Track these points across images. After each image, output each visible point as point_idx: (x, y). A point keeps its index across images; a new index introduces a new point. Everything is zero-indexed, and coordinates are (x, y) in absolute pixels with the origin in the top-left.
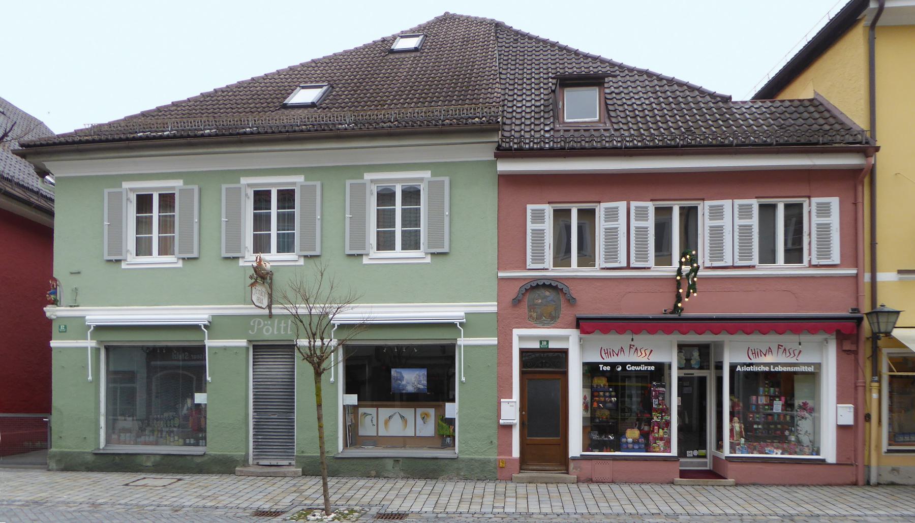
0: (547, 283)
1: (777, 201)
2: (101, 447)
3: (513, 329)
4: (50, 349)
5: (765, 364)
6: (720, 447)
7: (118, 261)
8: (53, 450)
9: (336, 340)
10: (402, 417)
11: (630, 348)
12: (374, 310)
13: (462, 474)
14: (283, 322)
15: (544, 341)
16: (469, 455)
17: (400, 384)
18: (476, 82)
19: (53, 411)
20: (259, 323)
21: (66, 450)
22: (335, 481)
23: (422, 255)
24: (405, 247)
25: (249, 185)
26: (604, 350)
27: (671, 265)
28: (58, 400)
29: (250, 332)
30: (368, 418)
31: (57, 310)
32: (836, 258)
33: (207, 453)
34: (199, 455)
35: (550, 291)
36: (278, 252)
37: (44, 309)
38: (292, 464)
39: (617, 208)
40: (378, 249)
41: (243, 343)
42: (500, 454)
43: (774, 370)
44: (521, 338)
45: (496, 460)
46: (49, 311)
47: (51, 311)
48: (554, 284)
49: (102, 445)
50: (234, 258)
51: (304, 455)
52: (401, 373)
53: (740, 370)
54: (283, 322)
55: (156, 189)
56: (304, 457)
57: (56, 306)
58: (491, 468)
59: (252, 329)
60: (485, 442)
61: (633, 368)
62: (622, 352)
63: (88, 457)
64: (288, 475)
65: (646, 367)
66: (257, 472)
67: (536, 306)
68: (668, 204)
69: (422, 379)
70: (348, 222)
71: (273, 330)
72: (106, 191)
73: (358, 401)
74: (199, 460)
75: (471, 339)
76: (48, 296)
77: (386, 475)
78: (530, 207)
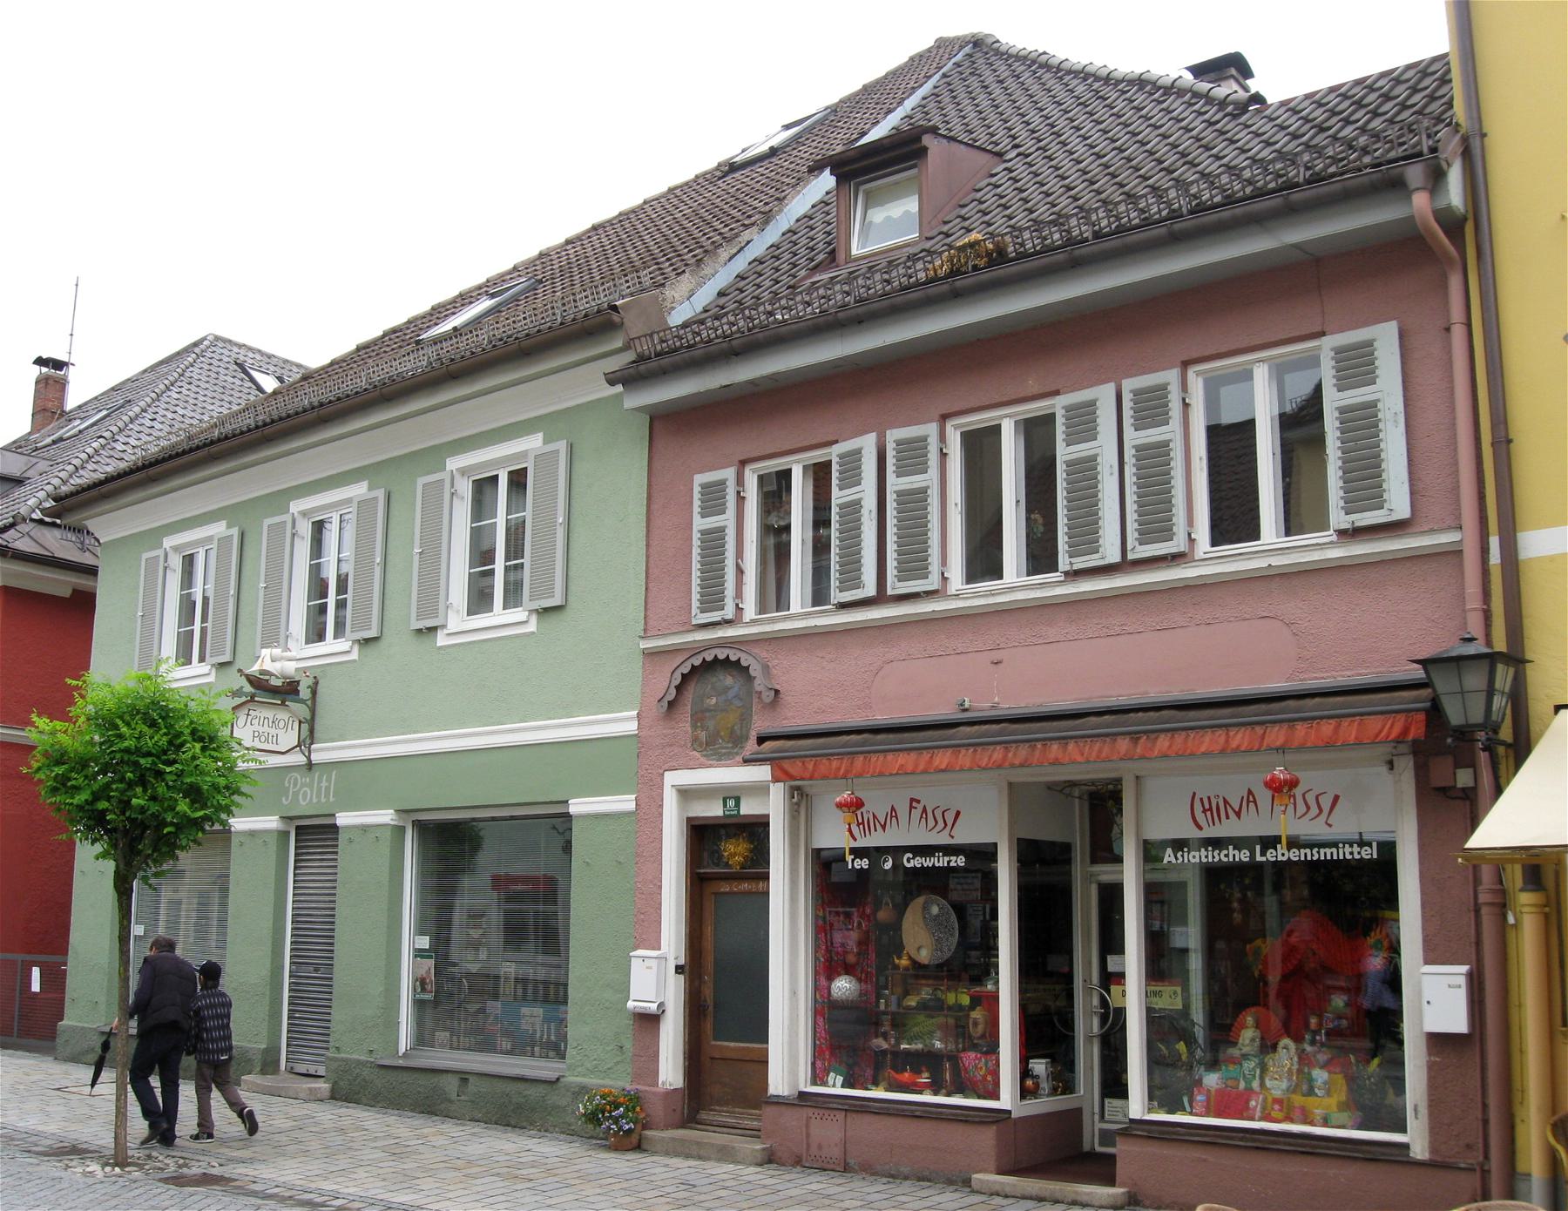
2: (402, 1050)
3: (666, 774)
5: (1239, 843)
6: (1115, 1086)
7: (433, 630)
9: (392, 811)
11: (911, 807)
26: (1201, 799)
32: (1398, 503)
34: (545, 1082)
35: (735, 673)
39: (1369, 344)
41: (386, 816)
43: (1264, 859)
44: (685, 794)
53: (1174, 861)
61: (917, 862)
62: (1252, 805)
65: (946, 859)
68: (1040, 409)
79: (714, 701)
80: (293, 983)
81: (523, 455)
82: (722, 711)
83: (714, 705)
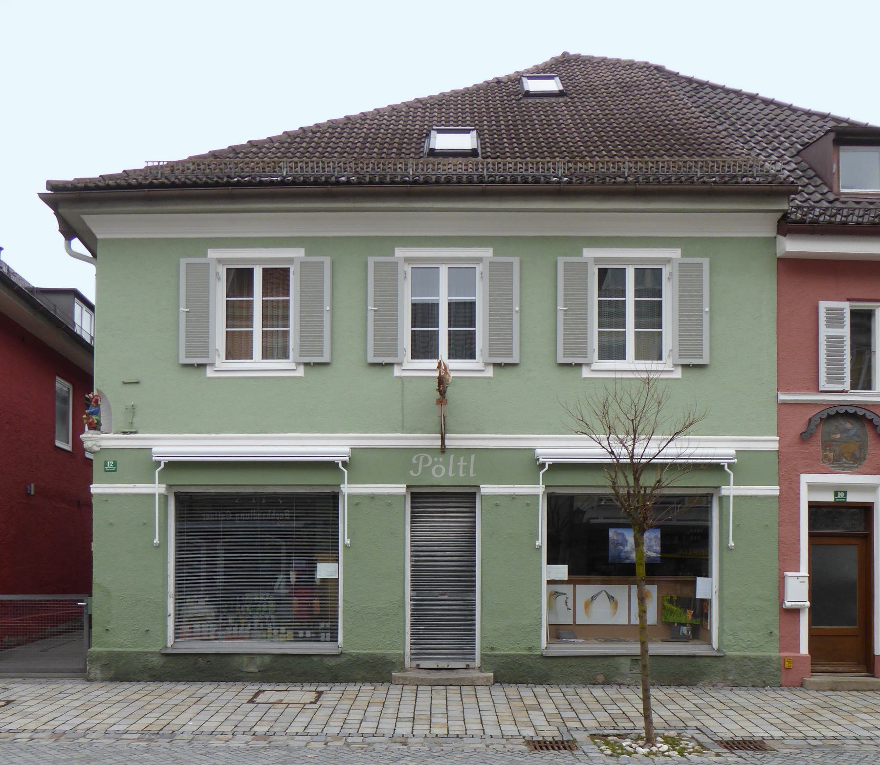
0: (851, 411)
1: (874, 306)
4: (90, 495)
8: (94, 649)
10: (611, 598)
12: (703, 444)
13: (731, 678)
14: (462, 458)
15: (840, 492)
16: (739, 651)
17: (620, 552)
18: (389, 126)
19: (95, 590)
20: (426, 461)
21: (116, 649)
22: (240, 687)
23: (292, 366)
24: (267, 354)
25: (220, 261)
27: (870, 389)
28: (100, 574)
29: (412, 473)
30: (561, 599)
31: (102, 439)
33: (344, 652)
35: (853, 422)
36: (227, 358)
37: (81, 436)
38: (470, 667)
40: (413, 357)
42: (782, 649)
44: (812, 487)
45: (780, 658)
46: (90, 439)
47: (91, 439)
48: (861, 412)
49: (170, 644)
50: (387, 364)
51: (497, 652)
52: (623, 535)
54: (462, 458)
55: (630, 261)
56: (496, 656)
57: (99, 432)
58: (773, 670)
59: (415, 468)
60: (760, 634)
63: (154, 659)
64: (477, 682)
66: (430, 680)
67: (834, 443)
69: (653, 543)
70: (371, 316)
71: (447, 471)
72: (183, 262)
73: (569, 574)
74: (332, 662)
75: (516, 486)
76: (85, 416)
77: (620, 681)
78: (823, 305)
79: (838, 436)
80: (413, 604)
81: (291, 260)
82: (845, 442)
83: (838, 439)
